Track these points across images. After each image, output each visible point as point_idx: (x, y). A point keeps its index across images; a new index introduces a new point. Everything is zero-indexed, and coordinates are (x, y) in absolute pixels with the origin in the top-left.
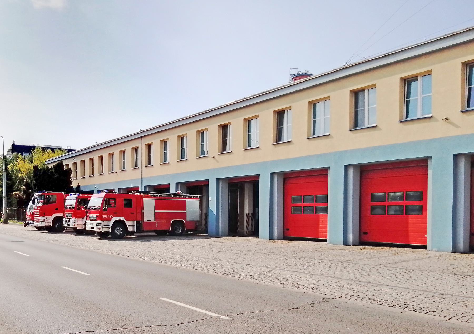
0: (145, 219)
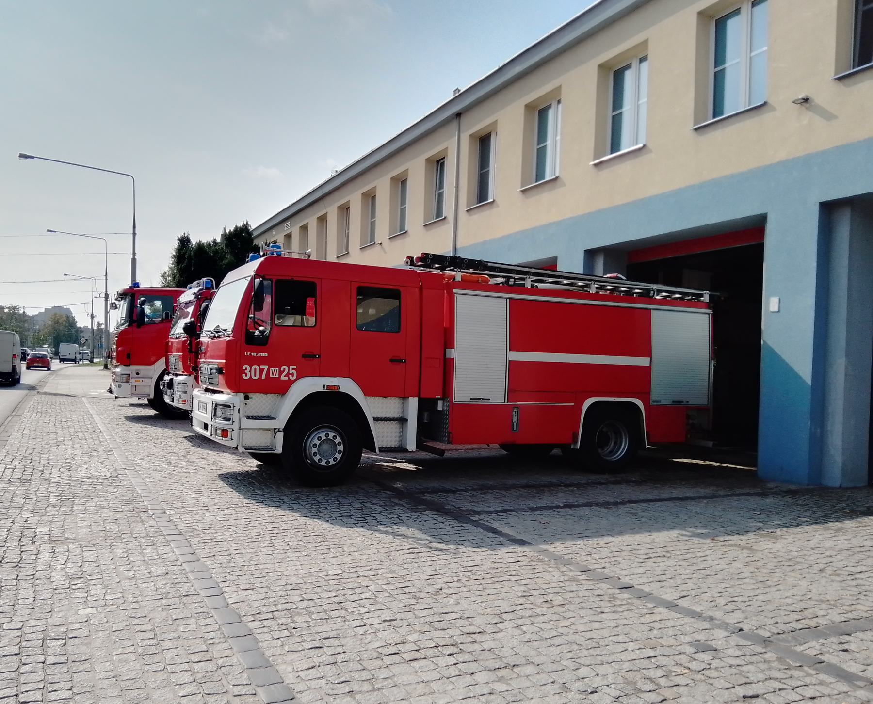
0: (462, 393)
